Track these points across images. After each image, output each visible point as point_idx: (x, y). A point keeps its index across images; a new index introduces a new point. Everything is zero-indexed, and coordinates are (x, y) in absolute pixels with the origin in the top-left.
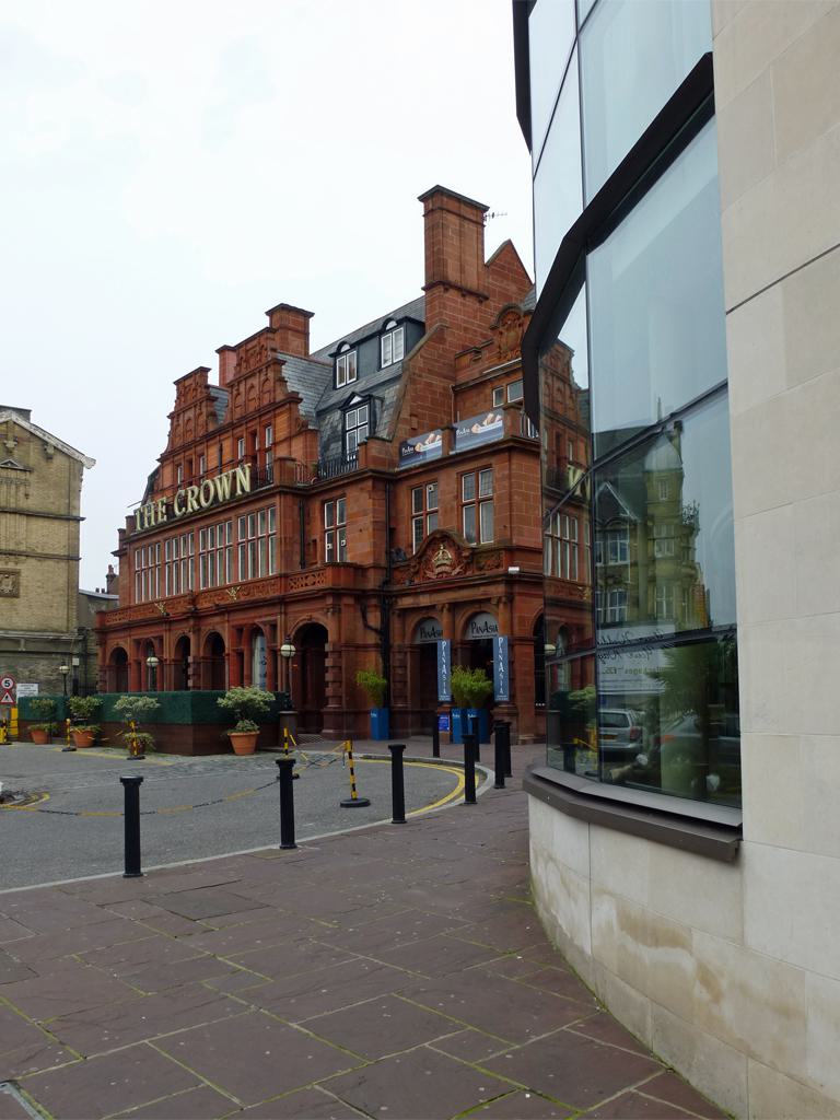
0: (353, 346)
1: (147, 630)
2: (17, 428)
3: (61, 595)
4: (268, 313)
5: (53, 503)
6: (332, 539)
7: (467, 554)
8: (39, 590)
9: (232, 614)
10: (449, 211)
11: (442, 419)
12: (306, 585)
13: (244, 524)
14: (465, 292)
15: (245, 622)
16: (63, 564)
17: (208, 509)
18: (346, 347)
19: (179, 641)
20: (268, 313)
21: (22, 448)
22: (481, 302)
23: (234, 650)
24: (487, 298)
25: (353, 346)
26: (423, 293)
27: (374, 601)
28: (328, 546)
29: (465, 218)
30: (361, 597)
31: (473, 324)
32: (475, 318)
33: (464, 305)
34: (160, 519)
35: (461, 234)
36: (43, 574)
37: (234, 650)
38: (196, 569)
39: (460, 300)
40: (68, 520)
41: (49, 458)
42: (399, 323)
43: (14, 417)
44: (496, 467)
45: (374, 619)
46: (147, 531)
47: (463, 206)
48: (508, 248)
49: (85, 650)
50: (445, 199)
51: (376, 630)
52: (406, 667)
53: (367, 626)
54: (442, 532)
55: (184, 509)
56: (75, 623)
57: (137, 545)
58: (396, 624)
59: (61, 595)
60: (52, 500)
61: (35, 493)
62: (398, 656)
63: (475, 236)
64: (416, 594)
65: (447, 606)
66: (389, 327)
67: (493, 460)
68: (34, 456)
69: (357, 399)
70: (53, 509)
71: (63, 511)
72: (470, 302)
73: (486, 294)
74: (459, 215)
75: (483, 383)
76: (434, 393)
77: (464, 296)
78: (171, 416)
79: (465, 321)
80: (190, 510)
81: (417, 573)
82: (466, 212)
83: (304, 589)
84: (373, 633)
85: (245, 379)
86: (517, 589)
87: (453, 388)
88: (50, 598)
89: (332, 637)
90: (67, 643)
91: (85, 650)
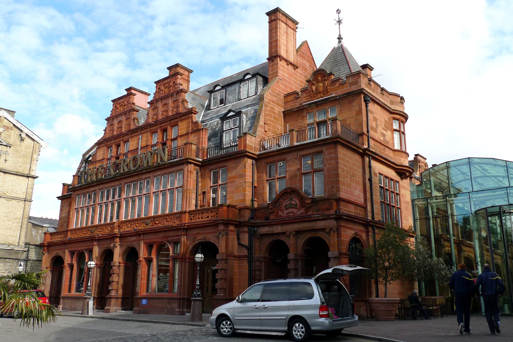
0: (223, 87)
1: (81, 244)
2: (5, 120)
3: (17, 223)
4: (168, 68)
5: (20, 166)
6: (215, 191)
7: (309, 202)
8: (5, 219)
9: (145, 236)
10: (282, 21)
11: (278, 127)
12: (202, 218)
13: (102, 193)
14: (289, 63)
15: (155, 240)
16: (22, 204)
17: (134, 171)
18: (218, 88)
19: (106, 250)
20: (168, 68)
21: (7, 133)
22: (295, 69)
23: (145, 258)
24: (297, 68)
25: (223, 87)
26: (267, 61)
27: (246, 229)
28: (212, 195)
29: (289, 26)
30: (239, 225)
31: (291, 80)
32: (292, 77)
33: (287, 69)
34: (99, 177)
35: (287, 33)
36: (8, 209)
37: (145, 258)
38: (88, 211)
39: (286, 66)
40: (28, 177)
41: (22, 140)
42: (254, 76)
43: (5, 114)
44: (326, 152)
45: (245, 238)
46: (89, 184)
47: (288, 20)
48: (305, 44)
49: (27, 257)
50: (281, 15)
51: (246, 247)
52: (261, 270)
53: (240, 244)
54: (291, 188)
55: (117, 171)
56: (23, 240)
57: (79, 192)
58: (256, 244)
59: (17, 223)
60: (20, 165)
61: (11, 160)
62: (258, 264)
63: (293, 36)
64: (271, 225)
65: (294, 233)
66: (216, 89)
67: (324, 148)
68: (13, 137)
69: (231, 114)
70: (21, 170)
71: (26, 172)
72: (290, 67)
73: (298, 66)
74: (287, 24)
75: (303, 109)
76: (274, 113)
77: (288, 65)
78: (108, 119)
79: (288, 78)
80: (122, 171)
81: (273, 212)
82: (290, 23)
83: (201, 220)
84: (245, 249)
85: (161, 100)
86: (342, 224)
87: (283, 112)
88: (11, 223)
89: (291, 249)
90: (17, 252)
91: (27, 257)
